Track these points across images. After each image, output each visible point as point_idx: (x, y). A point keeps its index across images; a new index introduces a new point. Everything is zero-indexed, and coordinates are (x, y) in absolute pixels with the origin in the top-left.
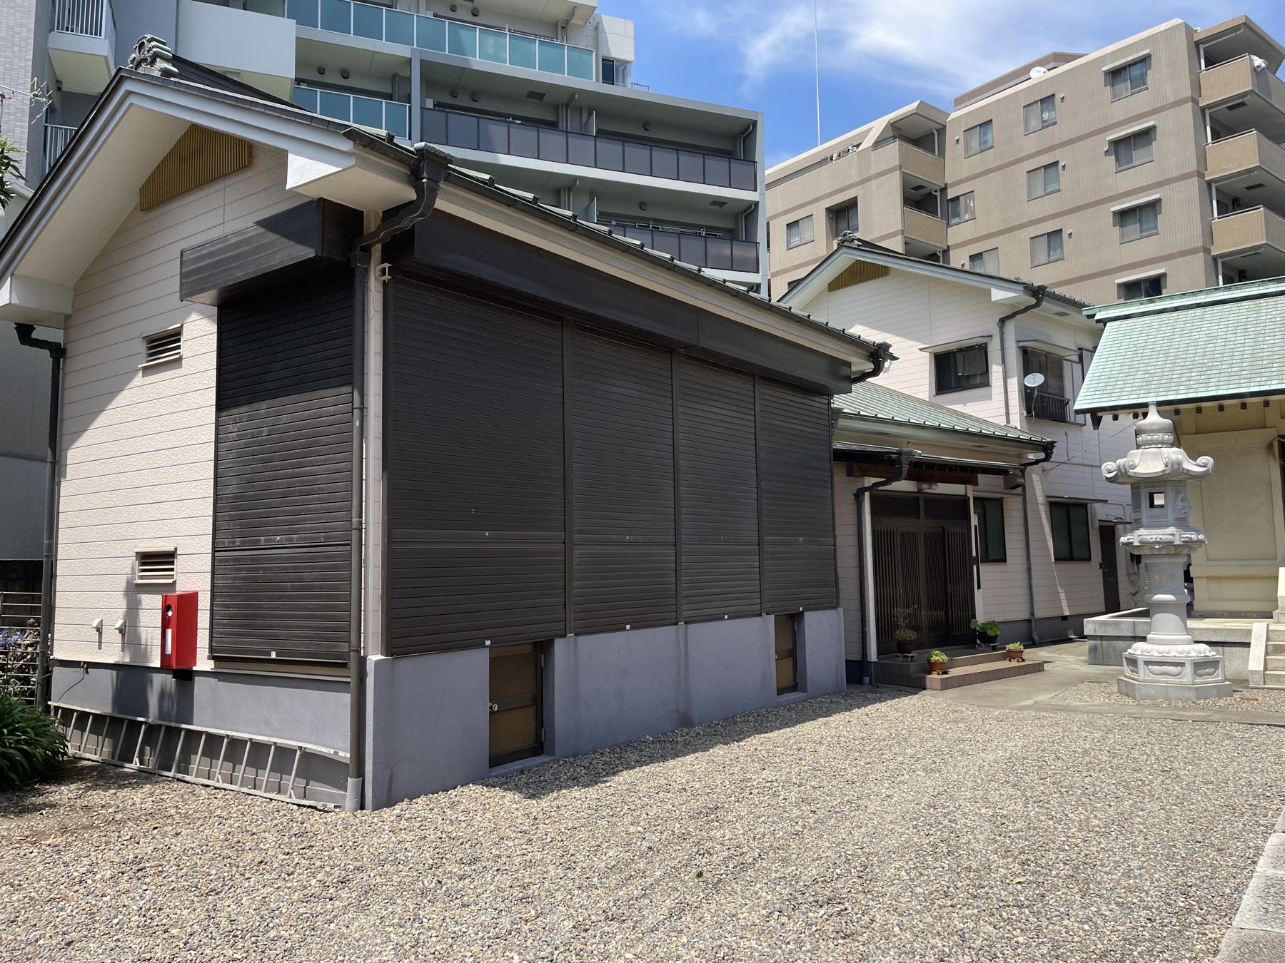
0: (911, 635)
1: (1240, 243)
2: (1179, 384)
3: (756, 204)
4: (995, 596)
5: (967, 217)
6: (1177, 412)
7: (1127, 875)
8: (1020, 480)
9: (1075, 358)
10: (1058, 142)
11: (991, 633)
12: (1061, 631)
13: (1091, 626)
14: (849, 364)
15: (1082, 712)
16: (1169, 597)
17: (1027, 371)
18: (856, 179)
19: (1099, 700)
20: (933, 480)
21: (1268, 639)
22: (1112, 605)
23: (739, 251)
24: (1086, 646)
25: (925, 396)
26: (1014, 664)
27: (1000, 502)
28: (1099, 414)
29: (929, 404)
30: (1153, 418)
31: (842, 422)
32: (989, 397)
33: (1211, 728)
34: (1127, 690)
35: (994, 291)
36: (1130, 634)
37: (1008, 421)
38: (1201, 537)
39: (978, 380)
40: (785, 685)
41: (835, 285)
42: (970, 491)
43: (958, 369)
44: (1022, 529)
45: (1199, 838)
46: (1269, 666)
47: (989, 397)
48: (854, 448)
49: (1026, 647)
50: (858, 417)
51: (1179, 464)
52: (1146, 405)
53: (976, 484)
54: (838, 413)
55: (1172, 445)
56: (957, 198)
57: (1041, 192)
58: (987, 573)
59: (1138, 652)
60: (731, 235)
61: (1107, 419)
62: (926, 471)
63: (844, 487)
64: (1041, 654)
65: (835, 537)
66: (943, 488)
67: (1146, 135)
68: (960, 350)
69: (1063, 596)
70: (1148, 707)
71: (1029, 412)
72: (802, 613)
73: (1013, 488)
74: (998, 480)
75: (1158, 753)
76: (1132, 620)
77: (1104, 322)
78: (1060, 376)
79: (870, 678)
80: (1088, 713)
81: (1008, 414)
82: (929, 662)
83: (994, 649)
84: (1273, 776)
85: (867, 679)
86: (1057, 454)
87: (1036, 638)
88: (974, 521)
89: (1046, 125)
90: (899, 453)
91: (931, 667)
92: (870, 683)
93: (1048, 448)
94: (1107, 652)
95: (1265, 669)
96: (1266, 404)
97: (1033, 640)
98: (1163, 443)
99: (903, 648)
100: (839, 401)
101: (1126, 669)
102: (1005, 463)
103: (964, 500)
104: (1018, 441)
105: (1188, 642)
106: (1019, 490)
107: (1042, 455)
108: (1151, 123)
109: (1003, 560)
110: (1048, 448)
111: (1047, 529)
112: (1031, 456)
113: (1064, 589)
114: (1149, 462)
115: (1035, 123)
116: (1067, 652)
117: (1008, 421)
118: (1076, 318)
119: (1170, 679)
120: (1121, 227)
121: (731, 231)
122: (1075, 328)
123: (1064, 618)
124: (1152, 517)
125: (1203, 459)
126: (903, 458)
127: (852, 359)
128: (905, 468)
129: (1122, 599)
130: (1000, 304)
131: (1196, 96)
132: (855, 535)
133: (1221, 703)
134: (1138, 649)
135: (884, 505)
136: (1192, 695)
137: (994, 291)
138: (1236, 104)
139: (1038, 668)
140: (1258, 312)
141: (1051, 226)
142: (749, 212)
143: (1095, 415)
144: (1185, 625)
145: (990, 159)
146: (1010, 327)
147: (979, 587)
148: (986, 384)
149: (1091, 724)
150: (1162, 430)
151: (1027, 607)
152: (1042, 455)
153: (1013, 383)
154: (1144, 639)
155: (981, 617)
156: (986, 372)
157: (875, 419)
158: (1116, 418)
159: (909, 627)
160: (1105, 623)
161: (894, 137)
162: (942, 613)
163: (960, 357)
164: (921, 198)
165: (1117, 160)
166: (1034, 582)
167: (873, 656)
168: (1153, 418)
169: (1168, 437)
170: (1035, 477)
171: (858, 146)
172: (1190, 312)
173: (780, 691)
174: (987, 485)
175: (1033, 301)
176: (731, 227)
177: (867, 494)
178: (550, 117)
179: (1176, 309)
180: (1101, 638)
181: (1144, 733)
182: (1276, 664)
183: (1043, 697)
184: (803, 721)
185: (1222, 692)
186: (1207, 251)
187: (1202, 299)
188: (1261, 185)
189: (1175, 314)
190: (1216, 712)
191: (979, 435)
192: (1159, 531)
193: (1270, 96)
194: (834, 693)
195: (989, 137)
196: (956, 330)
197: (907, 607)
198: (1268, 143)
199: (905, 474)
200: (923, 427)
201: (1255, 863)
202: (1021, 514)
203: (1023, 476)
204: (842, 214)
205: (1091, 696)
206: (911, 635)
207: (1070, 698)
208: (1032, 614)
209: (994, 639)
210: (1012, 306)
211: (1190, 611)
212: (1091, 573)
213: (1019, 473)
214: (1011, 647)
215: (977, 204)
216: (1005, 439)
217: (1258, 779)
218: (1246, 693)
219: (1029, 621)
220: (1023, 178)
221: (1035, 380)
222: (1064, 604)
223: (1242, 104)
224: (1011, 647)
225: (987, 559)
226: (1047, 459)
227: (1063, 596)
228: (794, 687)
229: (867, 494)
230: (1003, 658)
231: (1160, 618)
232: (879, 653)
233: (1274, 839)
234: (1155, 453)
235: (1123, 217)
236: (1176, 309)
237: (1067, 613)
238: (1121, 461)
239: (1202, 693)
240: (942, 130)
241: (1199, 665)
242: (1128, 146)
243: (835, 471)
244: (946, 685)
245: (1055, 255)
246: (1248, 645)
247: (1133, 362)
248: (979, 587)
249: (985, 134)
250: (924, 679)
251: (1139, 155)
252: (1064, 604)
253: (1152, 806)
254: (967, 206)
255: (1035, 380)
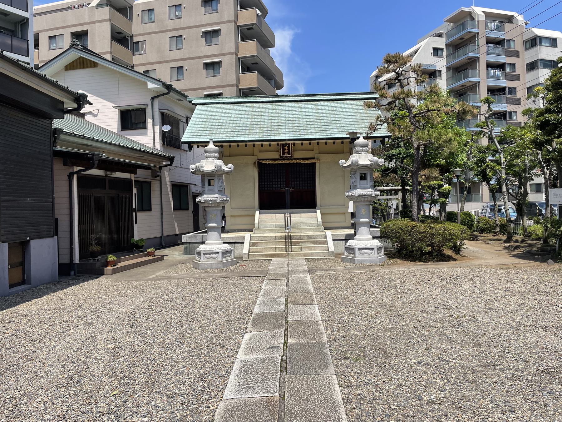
0: (98, 248)
1: (250, 85)
2: (223, 134)
3: (28, 19)
4: (143, 227)
5: (142, 52)
6: (222, 146)
7: (176, 374)
8: (159, 174)
9: (185, 121)
10: (182, 26)
11: (140, 244)
12: (173, 241)
13: (185, 238)
14: (63, 103)
15: (176, 279)
16: (215, 225)
17: (163, 124)
18: (87, 21)
19: (184, 272)
20: (113, 170)
21: (250, 240)
22: (196, 228)
23: (16, 43)
24: (182, 247)
25: (116, 131)
26: (150, 258)
27: (149, 183)
28: (192, 145)
29: (117, 134)
30: (211, 146)
31: (62, 137)
32: (146, 134)
33: (227, 280)
34: (196, 266)
35: (149, 83)
36: (200, 241)
37: (154, 146)
38: (228, 199)
39: (141, 125)
40: (17, 281)
41: (69, 67)
42: (133, 177)
43: (131, 119)
44: (159, 196)
45: (214, 342)
46: (251, 251)
47: (146, 134)
48: (69, 150)
49: (156, 250)
50: (72, 135)
51: (220, 167)
52: (208, 142)
53: (136, 173)
54: (58, 131)
55: (218, 159)
56: (138, 43)
57: (175, 48)
58: (141, 216)
59: (201, 249)
60: (13, 34)
61: (195, 147)
62: (109, 165)
63: (60, 172)
64: (165, 251)
65: (53, 198)
66: (118, 175)
67: (216, 33)
68: (133, 110)
69: (176, 225)
70: (204, 273)
71: (164, 143)
72: (29, 241)
73: (156, 177)
74: (149, 172)
75: (203, 296)
76: (202, 235)
77: (196, 105)
78: (178, 128)
79: (70, 273)
80: (178, 279)
81: (154, 143)
82: (107, 261)
83: (142, 252)
84: (248, 301)
85: (72, 273)
86: (176, 162)
87: (164, 244)
88: (135, 191)
89: (178, 17)
90: (93, 155)
91: (107, 264)
92: (74, 274)
93: (171, 159)
94: (191, 249)
95: (249, 252)
96: (254, 145)
97: (162, 245)
98: (215, 157)
99: (94, 255)
100: (57, 124)
101: (196, 256)
102: (154, 164)
103: (130, 181)
104: (158, 155)
105: (221, 244)
106: (158, 178)
107: (169, 163)
108: (219, 28)
109: (150, 210)
110: (171, 159)
111: (171, 196)
112: (164, 163)
113: (175, 223)
114: (209, 165)
115: (173, 16)
116: (176, 250)
117: (154, 146)
118: (185, 102)
119: (213, 260)
120: (207, 70)
121: (12, 31)
122: (185, 108)
123: (177, 235)
124: (209, 190)
125: (229, 166)
126: (95, 157)
127: (64, 100)
128: (96, 163)
129: (200, 226)
130: (151, 90)
131: (236, 20)
132: (67, 195)
133: (232, 268)
134: (202, 248)
135: (84, 182)
136: (221, 266)
137: (149, 83)
138: (250, 28)
139: (161, 259)
140: (253, 108)
141: (179, 64)
142: (24, 23)
143: (190, 145)
144: (220, 236)
145: (153, 27)
146: (156, 102)
147: (136, 223)
148: (145, 127)
149: (178, 285)
150: (214, 152)
151: (160, 231)
152: (169, 163)
153: (157, 128)
154: (203, 243)
155: (136, 237)
156: (145, 122)
157: (83, 137)
158: (198, 147)
159: (97, 244)
160: (191, 237)
161: (107, 5)
162: (116, 236)
163: (133, 113)
164: (120, 38)
165: (206, 41)
166: (164, 220)
167: (77, 260)
168: (211, 146)
169: (217, 155)
170: (166, 173)
171: (89, 4)
172: (229, 105)
173: (11, 286)
174: (141, 174)
175: (166, 91)
176: (13, 29)
177: (75, 176)
178: (11, 27)
179: (224, 103)
180: (189, 243)
181: (199, 286)
182: (253, 250)
183: (160, 273)
184: (24, 302)
185: (233, 263)
186: (237, 86)
187: (233, 100)
188: (256, 63)
189: (223, 105)
190: (230, 272)
191: (139, 151)
192: (212, 196)
193: (262, 27)
194: (50, 283)
195: (153, 16)
196: (132, 100)
197: (97, 233)
198: (260, 76)
199: (96, 165)
200: (110, 144)
201: (237, 352)
202: (159, 189)
203: (161, 172)
204: (80, 36)
205: (181, 270)
206: (98, 248)
207: (173, 273)
208: (163, 234)
209: (142, 247)
210: (157, 92)
211: (223, 230)
212: (188, 215)
213: (159, 171)
214: (149, 250)
215: (147, 46)
216: (152, 154)
217: (243, 304)
218: (242, 263)
219: (161, 237)
220: (168, 39)
221: (167, 128)
222: (177, 229)
223: (252, 28)
224: (149, 250)
225: (142, 210)
226: (171, 165)
227: (176, 225)
228: (23, 282)
229: (75, 176)
230: (146, 255)
231: (210, 233)
232: (81, 258)
233: (247, 336)
234: (212, 162)
235: (208, 66)
236: (224, 103)
237: (178, 233)
238: (197, 164)
239: (225, 265)
240: (131, 8)
241: (226, 253)
242: (211, 35)
243: (54, 162)
244: (114, 272)
245: (180, 78)
246: (243, 243)
247: (206, 124)
248: (136, 223)
249: (151, 15)
250: (104, 269)
251: (214, 40)
252: (177, 229)
253: (196, 326)
254: (142, 47)
255: (167, 128)
